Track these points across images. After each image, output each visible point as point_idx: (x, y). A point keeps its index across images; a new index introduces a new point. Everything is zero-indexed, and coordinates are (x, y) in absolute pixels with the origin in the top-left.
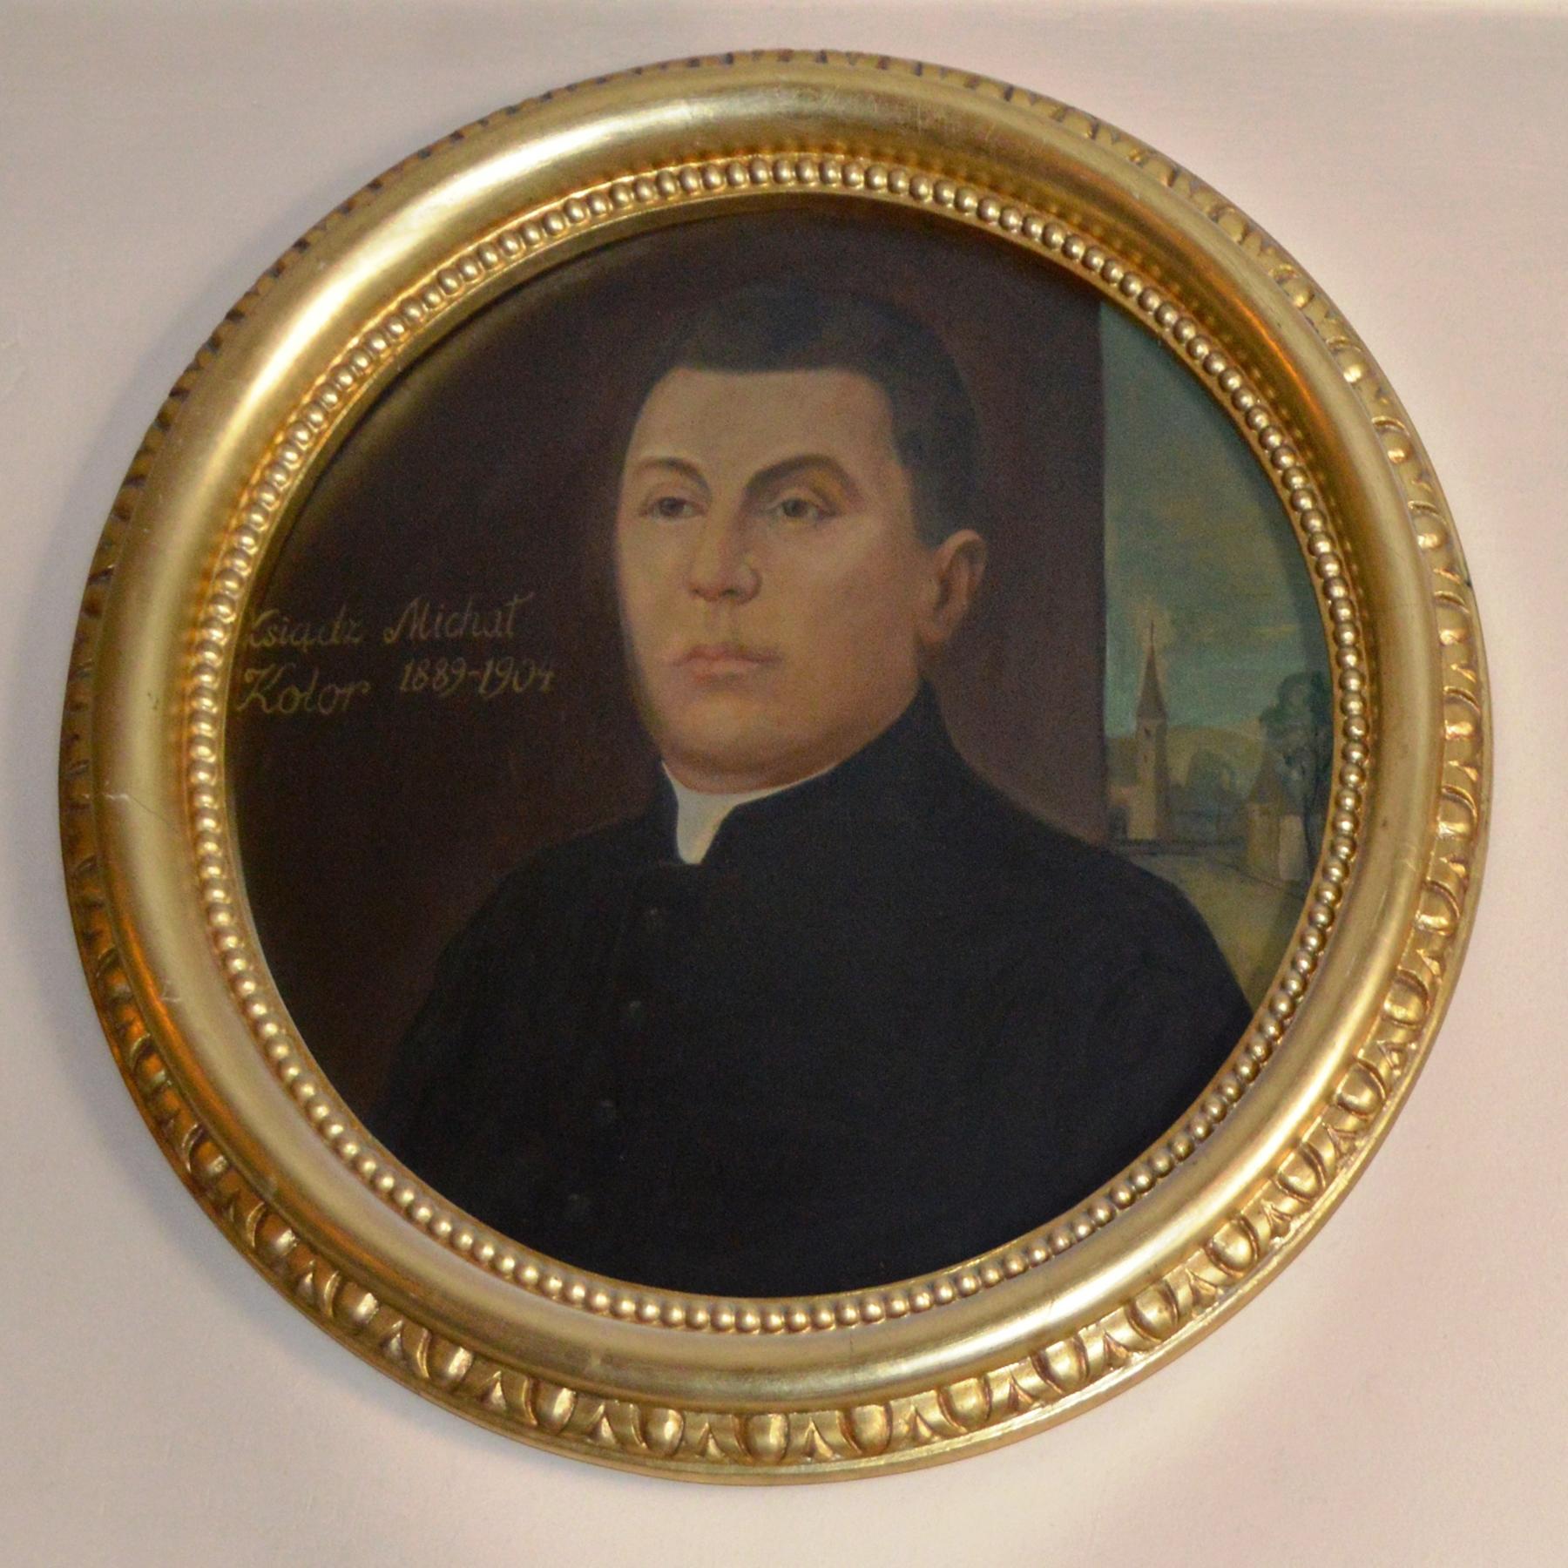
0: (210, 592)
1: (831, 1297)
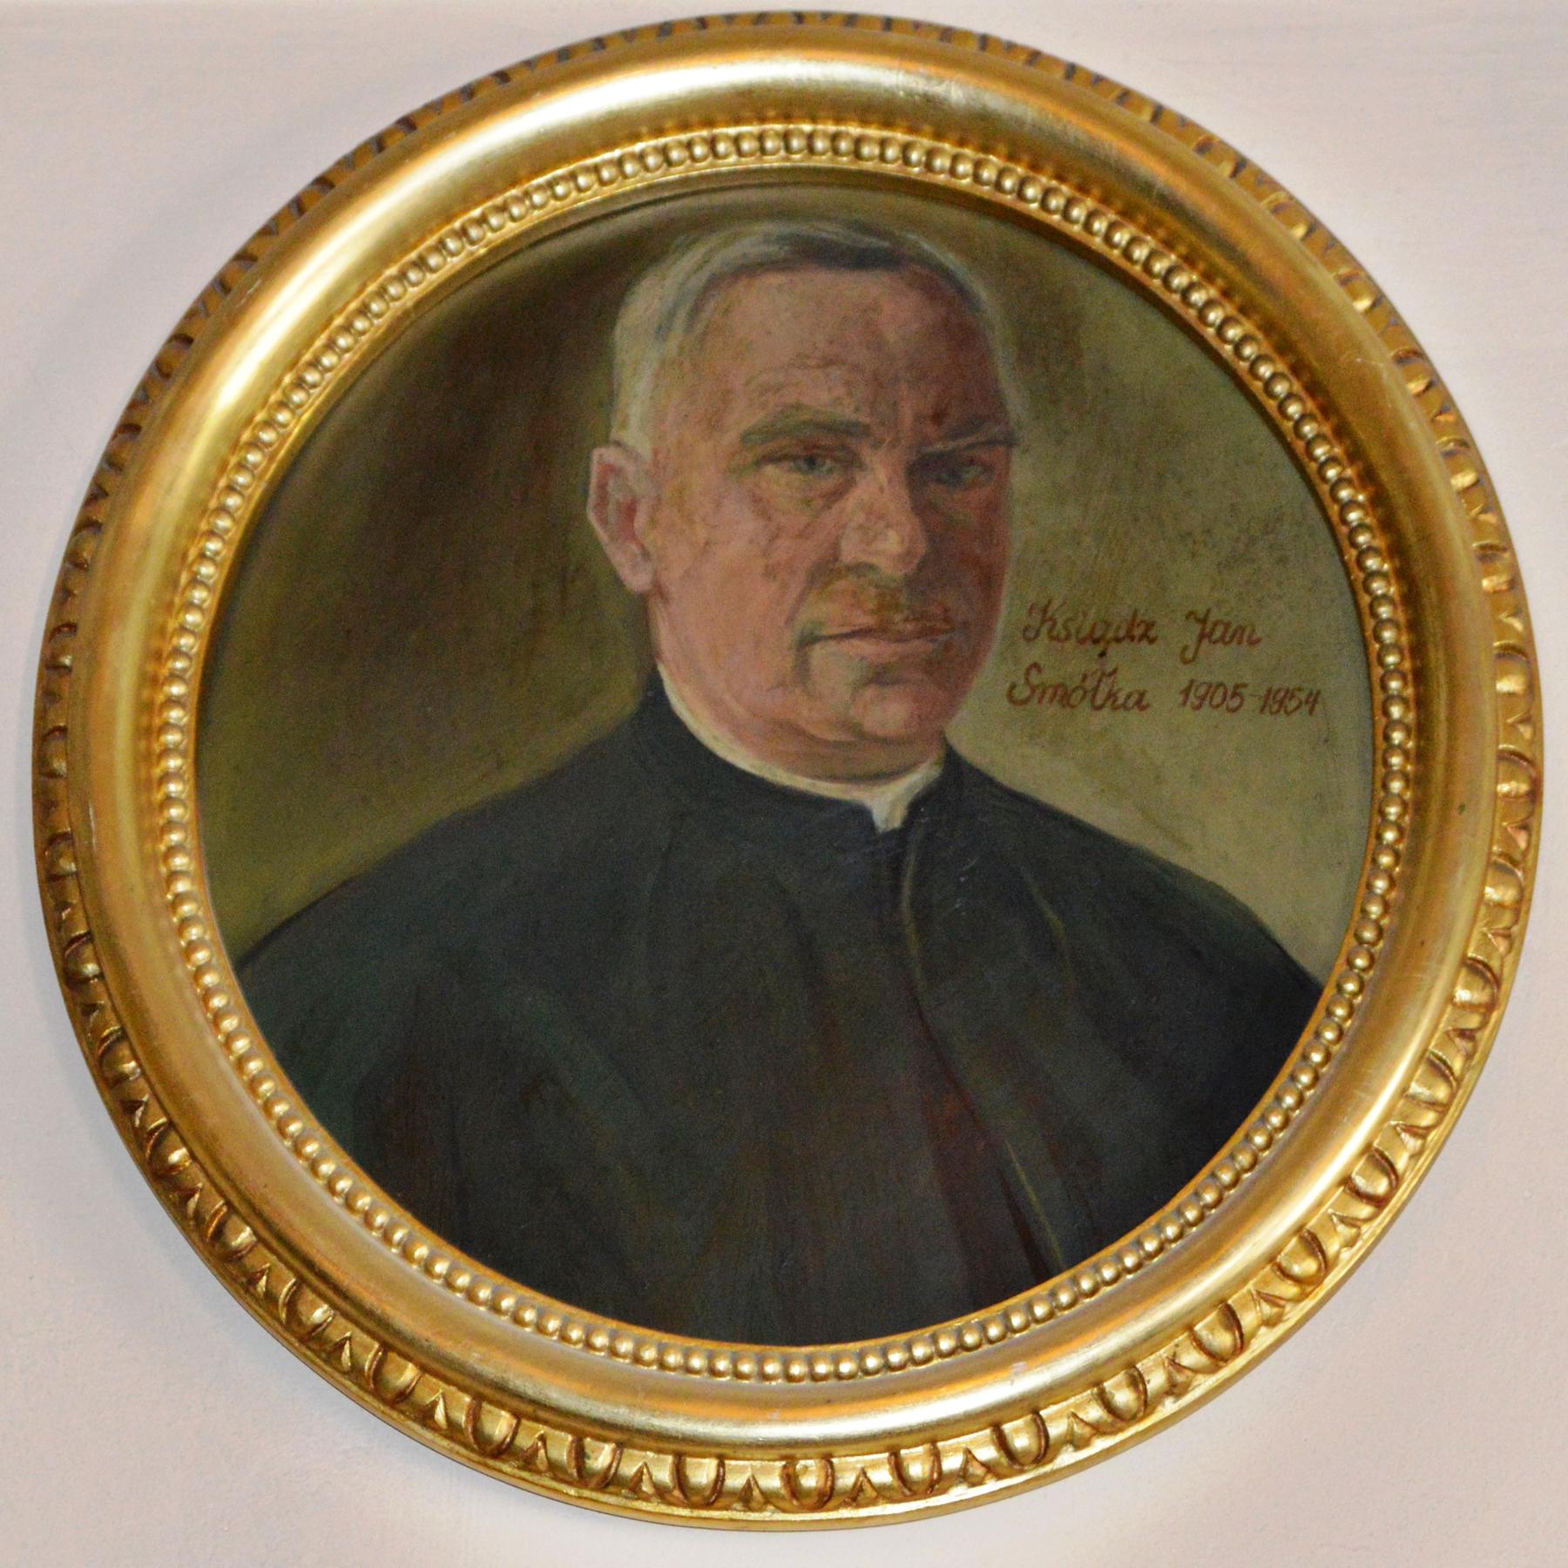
0: (157, 748)
1: (757, 1348)
